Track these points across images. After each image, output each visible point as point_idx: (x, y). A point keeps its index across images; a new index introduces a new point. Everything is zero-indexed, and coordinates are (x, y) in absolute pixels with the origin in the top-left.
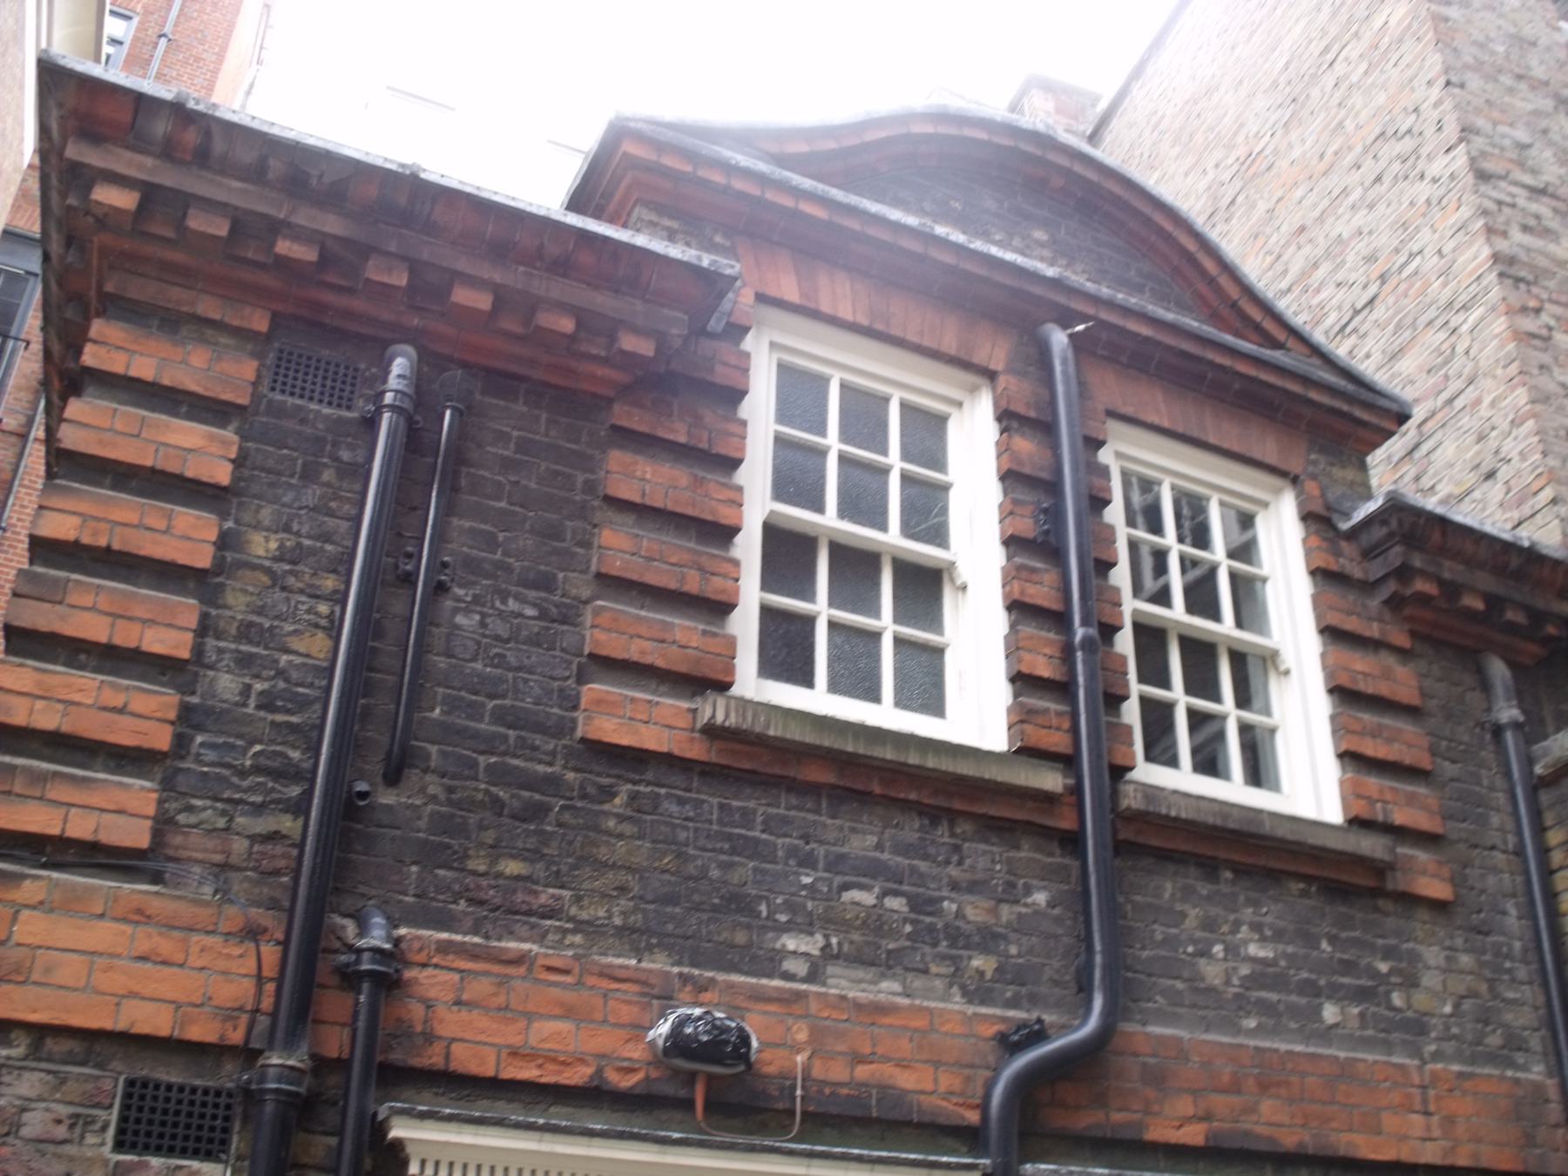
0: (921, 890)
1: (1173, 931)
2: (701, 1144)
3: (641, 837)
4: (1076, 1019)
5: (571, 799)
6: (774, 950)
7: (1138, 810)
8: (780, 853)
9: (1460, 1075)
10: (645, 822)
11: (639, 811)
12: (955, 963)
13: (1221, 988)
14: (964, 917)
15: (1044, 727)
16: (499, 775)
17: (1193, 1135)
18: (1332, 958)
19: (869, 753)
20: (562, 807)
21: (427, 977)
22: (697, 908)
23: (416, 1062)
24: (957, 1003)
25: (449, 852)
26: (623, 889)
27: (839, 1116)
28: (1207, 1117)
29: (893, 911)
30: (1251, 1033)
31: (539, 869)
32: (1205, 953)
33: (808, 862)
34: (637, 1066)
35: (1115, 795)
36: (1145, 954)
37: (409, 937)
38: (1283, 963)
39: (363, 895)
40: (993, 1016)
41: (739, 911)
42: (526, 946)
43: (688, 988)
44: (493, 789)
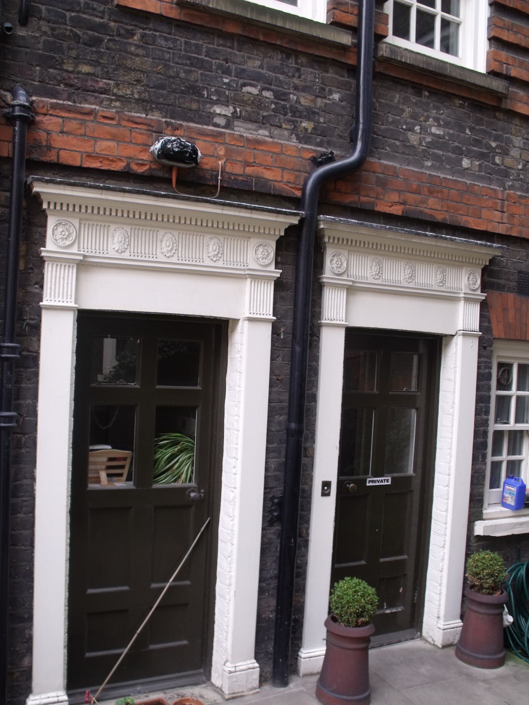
0: (280, 89)
1: (397, 117)
2: (174, 197)
3: (147, 56)
4: (348, 154)
5: (113, 36)
6: (210, 112)
7: (387, 57)
8: (214, 67)
9: (520, 196)
10: (149, 49)
11: (146, 43)
12: (294, 124)
13: (417, 146)
14: (300, 102)
15: (345, 12)
16: (77, 22)
17: (397, 210)
18: (470, 137)
19: (258, 19)
20: (109, 40)
21: (47, 120)
22: (174, 91)
23: (44, 159)
24: (294, 142)
25: (54, 60)
26: (138, 81)
27: (238, 189)
28: (404, 203)
29: (266, 97)
30: (428, 168)
31: (98, 70)
32: (411, 130)
33: (227, 72)
34: (146, 163)
35: (376, 49)
36: (383, 127)
37: (37, 101)
38: (447, 138)
39: (14, 80)
40: (311, 149)
41: (194, 93)
42: (93, 107)
43: (170, 128)
44: (73, 29)
